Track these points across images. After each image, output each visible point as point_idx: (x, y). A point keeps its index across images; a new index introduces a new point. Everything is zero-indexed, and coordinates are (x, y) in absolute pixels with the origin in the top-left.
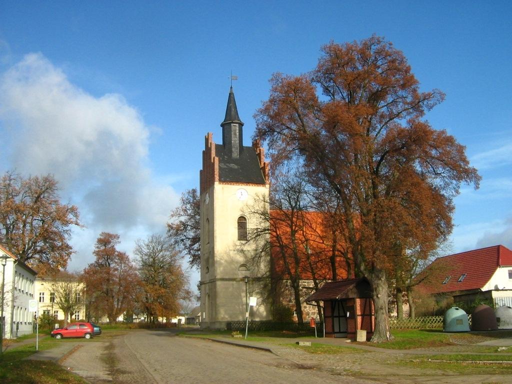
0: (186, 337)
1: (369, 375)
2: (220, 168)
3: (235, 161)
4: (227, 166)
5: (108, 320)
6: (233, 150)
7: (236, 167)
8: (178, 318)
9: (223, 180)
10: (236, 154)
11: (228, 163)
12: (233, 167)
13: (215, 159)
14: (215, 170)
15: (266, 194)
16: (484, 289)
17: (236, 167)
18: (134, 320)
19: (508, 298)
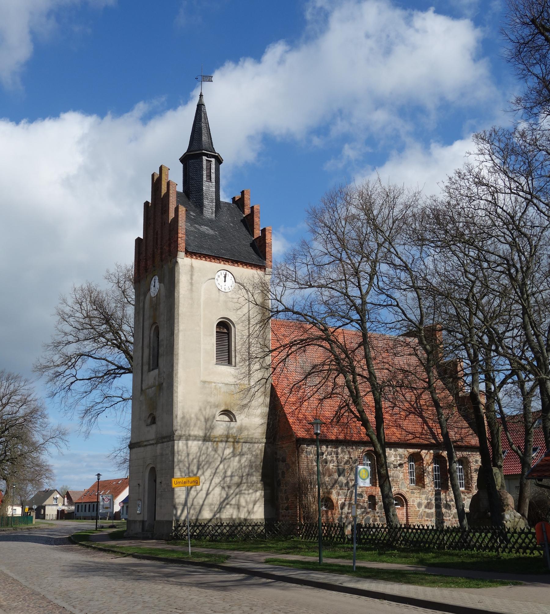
0: (200, 585)
1: (174, 584)
2: (187, 233)
3: (210, 223)
4: (196, 228)
5: (258, 514)
6: (206, 202)
7: (211, 232)
8: (532, 555)
9: (189, 253)
10: (209, 211)
11: (197, 224)
12: (207, 232)
13: (180, 210)
14: (180, 231)
15: (406, 192)
16: (43, 505)
17: (211, 232)
18: (447, 524)
19: (84, 510)
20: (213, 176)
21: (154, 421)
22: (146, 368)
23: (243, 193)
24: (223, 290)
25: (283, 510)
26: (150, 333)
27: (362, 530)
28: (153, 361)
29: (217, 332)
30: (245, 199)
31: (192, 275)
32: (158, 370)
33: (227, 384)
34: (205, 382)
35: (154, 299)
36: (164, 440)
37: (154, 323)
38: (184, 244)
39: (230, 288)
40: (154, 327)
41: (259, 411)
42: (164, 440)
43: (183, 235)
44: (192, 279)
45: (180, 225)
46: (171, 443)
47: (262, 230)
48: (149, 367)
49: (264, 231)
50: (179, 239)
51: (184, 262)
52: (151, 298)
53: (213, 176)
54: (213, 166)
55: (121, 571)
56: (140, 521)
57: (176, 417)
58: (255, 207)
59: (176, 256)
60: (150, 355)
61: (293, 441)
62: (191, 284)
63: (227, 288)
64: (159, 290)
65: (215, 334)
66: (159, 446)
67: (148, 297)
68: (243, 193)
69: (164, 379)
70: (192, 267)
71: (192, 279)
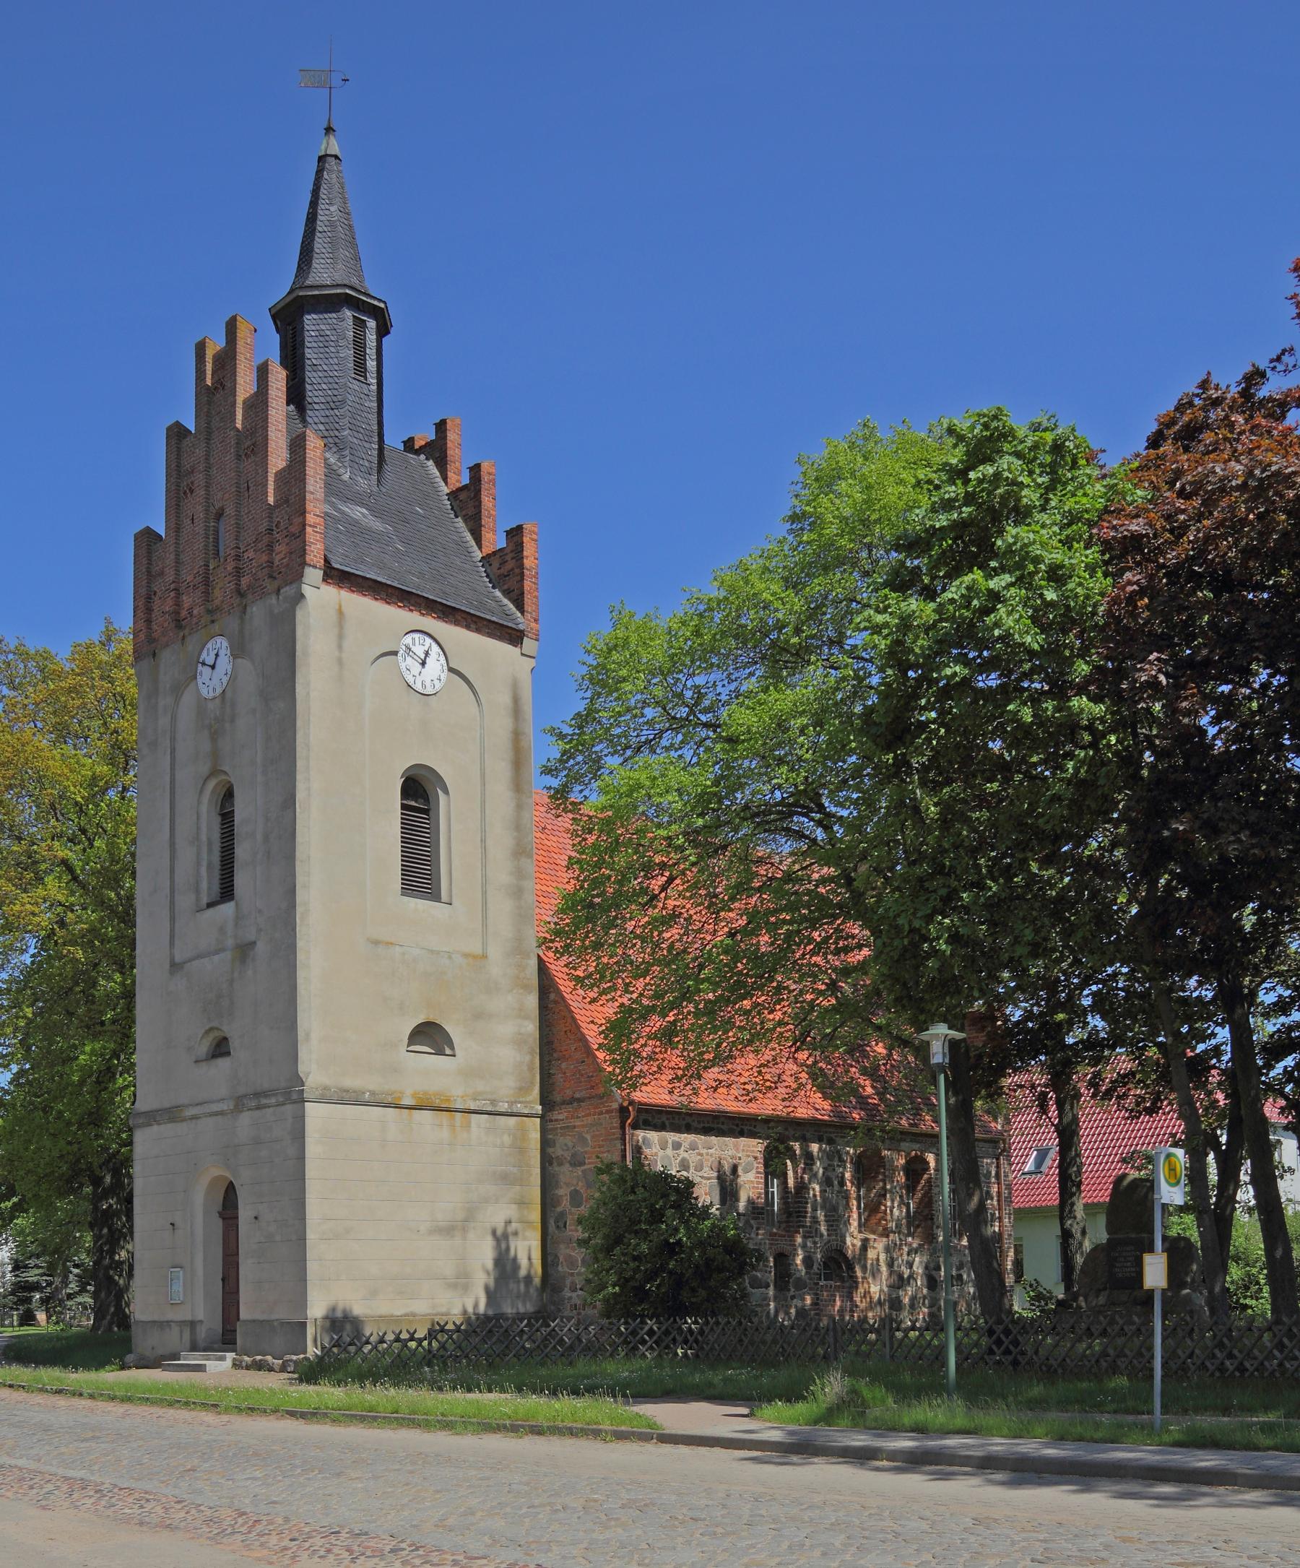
9: (334, 575)
20: (371, 364)
21: (221, 1049)
22: (185, 901)
23: (441, 427)
24: (418, 687)
25: (574, 1290)
26: (199, 802)
27: (899, 1335)
28: (209, 883)
29: (404, 807)
30: (449, 444)
31: (341, 637)
32: (232, 904)
33: (432, 951)
34: (376, 943)
35: (211, 706)
36: (264, 1101)
37: (214, 772)
38: (320, 546)
39: (436, 682)
40: (211, 784)
41: (507, 1029)
42: (264, 1101)
43: (318, 520)
44: (340, 647)
45: (309, 488)
46: (289, 1108)
47: (508, 533)
48: (198, 900)
49: (515, 534)
50: (309, 529)
51: (319, 597)
52: (201, 702)
53: (371, 364)
54: (371, 338)
55: (1003, 1483)
56: (182, 1323)
57: (308, 1035)
58: (485, 467)
59: (299, 577)
60: (198, 864)
61: (611, 1111)
62: (340, 662)
63: (428, 684)
64: (233, 679)
65: (399, 811)
66: (245, 1118)
67: (188, 698)
68: (441, 427)
69: (259, 931)
70: (340, 612)
71: (340, 647)
